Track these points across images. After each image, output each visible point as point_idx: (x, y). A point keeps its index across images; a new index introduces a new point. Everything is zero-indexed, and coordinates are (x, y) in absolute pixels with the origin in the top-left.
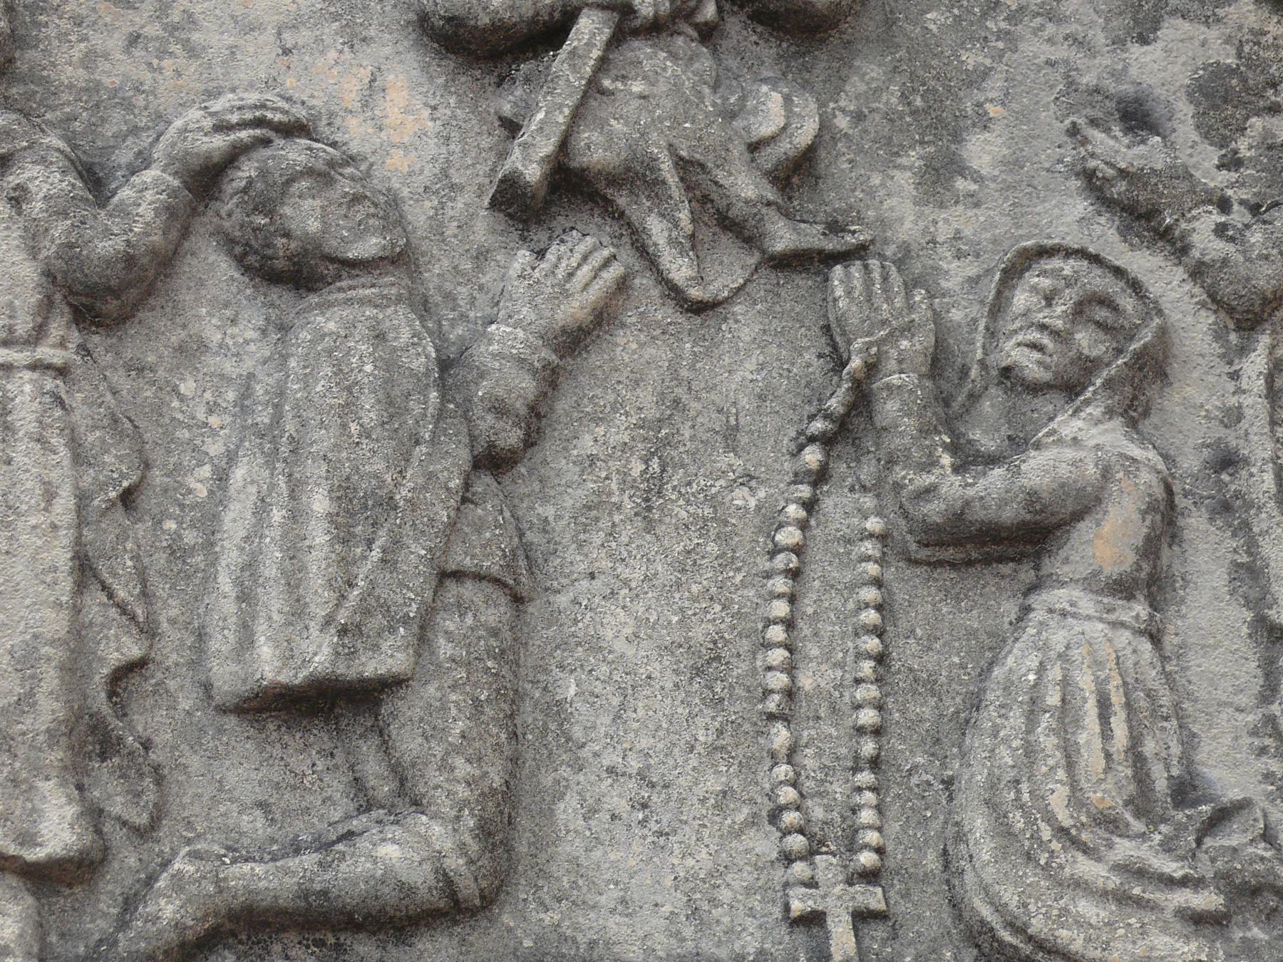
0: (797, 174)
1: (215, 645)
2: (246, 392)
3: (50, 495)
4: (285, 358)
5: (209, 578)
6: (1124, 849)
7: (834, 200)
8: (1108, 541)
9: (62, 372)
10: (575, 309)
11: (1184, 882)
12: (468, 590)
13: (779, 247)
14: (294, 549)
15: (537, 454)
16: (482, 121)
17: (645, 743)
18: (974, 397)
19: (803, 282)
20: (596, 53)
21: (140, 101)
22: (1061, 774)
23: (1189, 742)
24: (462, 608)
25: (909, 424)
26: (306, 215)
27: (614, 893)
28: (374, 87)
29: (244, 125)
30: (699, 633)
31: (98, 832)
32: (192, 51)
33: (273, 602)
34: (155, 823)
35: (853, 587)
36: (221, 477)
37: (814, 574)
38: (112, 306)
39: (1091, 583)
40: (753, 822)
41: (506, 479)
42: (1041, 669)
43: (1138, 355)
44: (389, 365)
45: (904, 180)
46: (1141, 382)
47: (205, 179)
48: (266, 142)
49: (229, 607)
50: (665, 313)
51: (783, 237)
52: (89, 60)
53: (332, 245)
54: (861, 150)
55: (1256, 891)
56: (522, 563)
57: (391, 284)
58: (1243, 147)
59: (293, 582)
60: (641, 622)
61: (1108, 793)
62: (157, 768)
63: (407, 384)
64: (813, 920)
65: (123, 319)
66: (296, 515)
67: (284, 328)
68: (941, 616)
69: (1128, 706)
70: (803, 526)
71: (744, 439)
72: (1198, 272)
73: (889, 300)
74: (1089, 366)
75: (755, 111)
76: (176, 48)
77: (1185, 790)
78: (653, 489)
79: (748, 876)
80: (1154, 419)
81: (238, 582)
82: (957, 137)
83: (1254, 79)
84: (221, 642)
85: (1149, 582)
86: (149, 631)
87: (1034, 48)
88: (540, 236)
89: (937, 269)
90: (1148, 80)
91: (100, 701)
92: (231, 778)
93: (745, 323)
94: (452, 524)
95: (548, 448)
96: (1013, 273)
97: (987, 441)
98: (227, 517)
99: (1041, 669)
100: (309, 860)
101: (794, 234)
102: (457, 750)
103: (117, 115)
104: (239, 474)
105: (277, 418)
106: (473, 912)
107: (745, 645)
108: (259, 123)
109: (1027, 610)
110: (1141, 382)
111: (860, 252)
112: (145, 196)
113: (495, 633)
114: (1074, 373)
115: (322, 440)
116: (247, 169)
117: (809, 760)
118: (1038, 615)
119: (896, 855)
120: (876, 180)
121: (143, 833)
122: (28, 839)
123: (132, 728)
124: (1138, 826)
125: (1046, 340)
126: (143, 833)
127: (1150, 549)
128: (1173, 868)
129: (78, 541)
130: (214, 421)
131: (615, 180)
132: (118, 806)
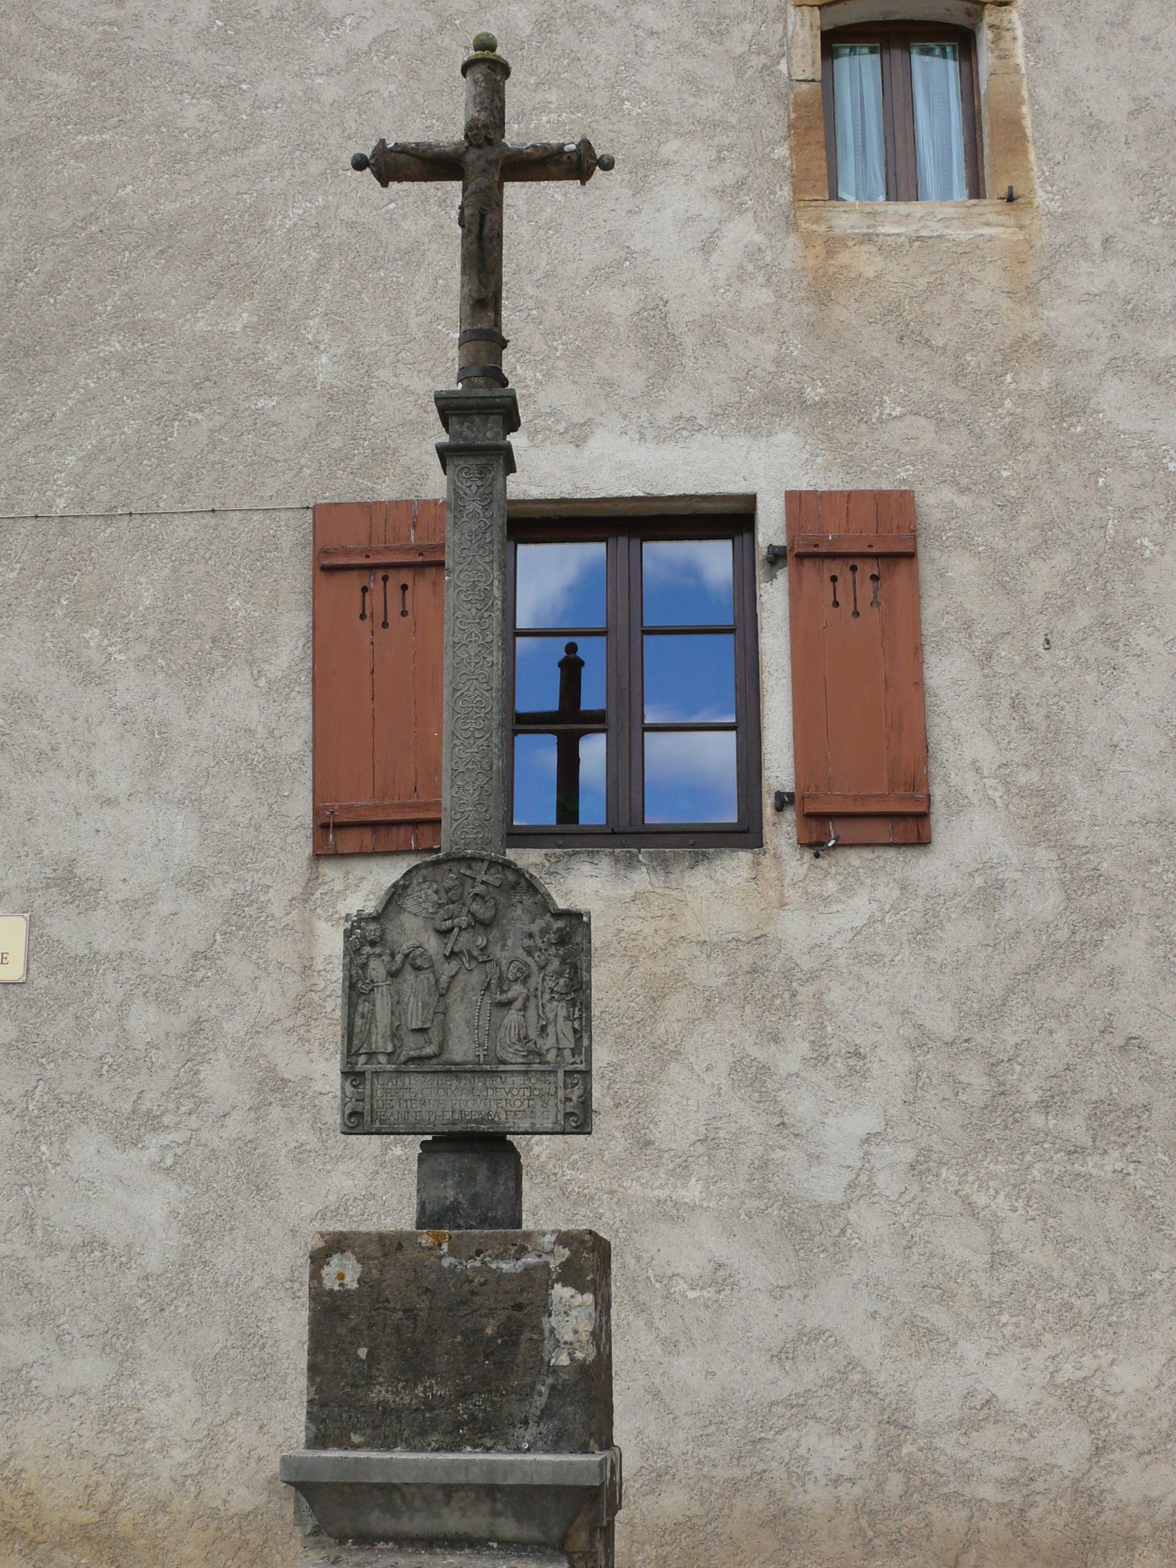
0: (484, 949)
8: (518, 1004)
10: (453, 973)
26: (419, 962)
44: (429, 983)
47: (407, 956)
68: (498, 1013)
85: (524, 1008)
87: (518, 925)
93: (476, 972)
97: (505, 988)
101: (483, 958)
112: (399, 957)
127: (524, 1004)
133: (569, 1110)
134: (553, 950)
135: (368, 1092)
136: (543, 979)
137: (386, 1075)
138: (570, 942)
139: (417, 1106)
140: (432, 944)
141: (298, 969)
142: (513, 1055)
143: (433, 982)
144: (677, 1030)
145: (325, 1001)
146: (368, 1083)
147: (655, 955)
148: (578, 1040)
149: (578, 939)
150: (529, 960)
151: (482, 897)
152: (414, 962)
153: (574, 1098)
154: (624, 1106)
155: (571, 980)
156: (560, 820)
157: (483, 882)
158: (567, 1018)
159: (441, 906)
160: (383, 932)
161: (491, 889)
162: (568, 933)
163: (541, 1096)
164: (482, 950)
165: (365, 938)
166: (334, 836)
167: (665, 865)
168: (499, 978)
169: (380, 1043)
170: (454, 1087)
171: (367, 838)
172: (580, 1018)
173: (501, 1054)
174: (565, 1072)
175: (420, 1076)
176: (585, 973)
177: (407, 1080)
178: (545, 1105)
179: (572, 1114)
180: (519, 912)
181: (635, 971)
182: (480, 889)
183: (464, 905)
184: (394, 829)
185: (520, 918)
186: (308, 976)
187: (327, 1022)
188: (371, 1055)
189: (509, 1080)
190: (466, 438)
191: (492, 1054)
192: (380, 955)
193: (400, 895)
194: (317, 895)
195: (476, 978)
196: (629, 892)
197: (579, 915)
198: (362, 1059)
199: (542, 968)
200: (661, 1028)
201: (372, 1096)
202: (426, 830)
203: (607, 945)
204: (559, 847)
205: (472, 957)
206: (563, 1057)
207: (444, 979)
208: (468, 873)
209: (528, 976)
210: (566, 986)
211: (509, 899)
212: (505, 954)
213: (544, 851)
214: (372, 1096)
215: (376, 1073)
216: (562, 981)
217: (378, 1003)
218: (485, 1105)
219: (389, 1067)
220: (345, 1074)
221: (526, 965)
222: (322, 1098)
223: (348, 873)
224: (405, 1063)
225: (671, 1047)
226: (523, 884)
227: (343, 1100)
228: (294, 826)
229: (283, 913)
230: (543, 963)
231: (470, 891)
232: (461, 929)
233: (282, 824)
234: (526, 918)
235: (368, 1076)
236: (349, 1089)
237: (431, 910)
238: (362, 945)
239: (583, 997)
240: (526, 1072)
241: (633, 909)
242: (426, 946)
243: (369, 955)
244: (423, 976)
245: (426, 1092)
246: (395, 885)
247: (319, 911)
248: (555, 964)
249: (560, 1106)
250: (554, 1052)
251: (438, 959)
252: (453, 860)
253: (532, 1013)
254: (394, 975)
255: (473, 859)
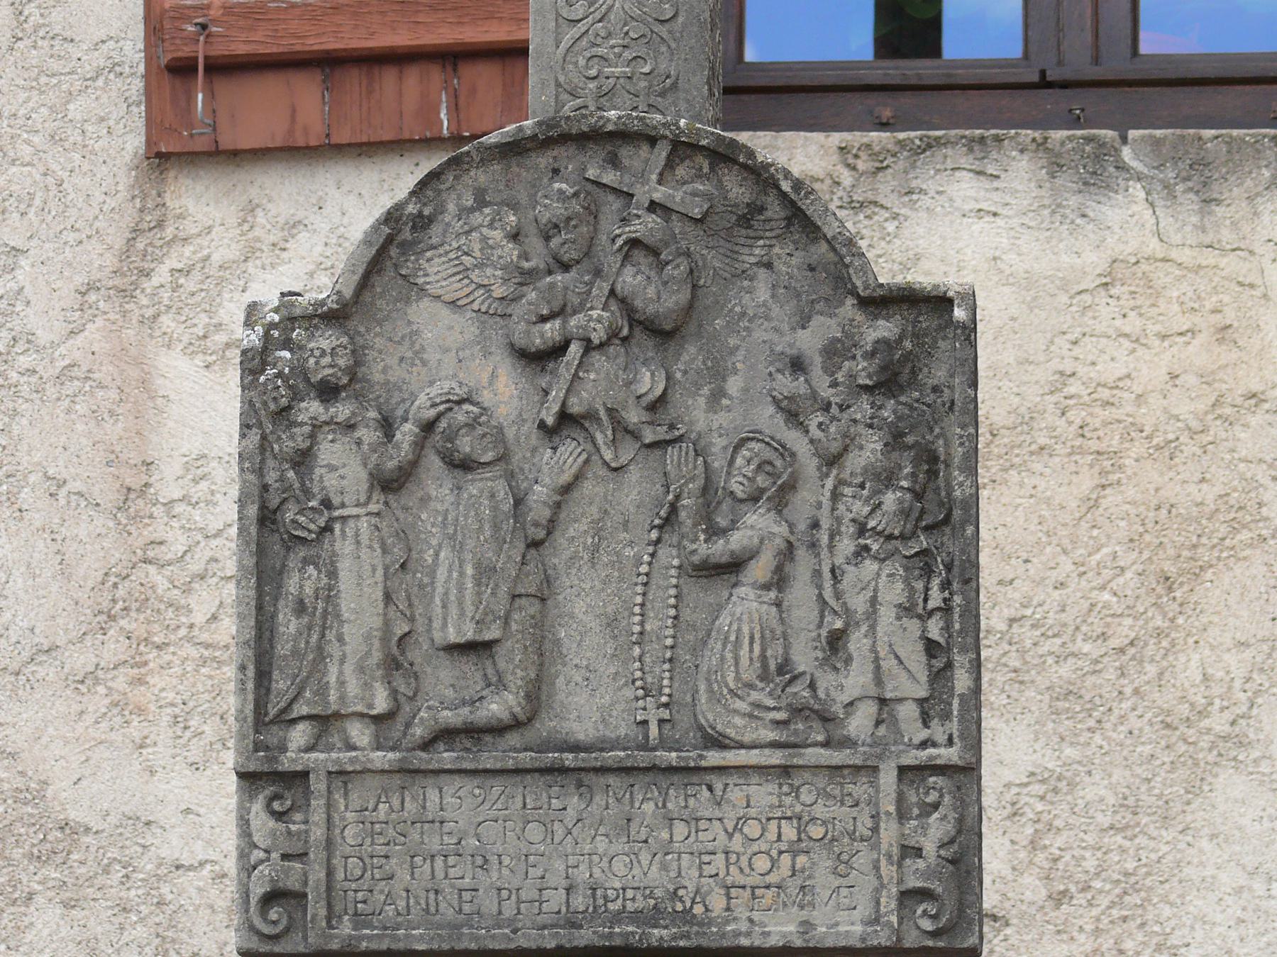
0: (656, 406)
1: (435, 625)
2: (445, 519)
3: (374, 570)
4: (459, 504)
5: (433, 597)
6: (755, 696)
7: (673, 413)
8: (760, 569)
9: (378, 514)
10: (566, 477)
11: (774, 708)
12: (523, 601)
13: (647, 441)
14: (461, 589)
15: (552, 537)
16: (535, 389)
17: (588, 655)
18: (719, 503)
19: (658, 452)
20: (576, 362)
21: (405, 387)
22: (732, 668)
23: (787, 647)
24: (521, 609)
25: (689, 522)
26: (465, 444)
27: (575, 713)
28: (493, 376)
29: (442, 403)
30: (609, 610)
31: (396, 700)
32: (424, 363)
33: (454, 611)
34: (415, 695)
35: (667, 588)
36: (437, 554)
37: (653, 582)
38: (396, 485)
39: (754, 585)
40: (626, 684)
41: (541, 549)
42: (730, 625)
43: (780, 486)
44: (495, 509)
45: (702, 401)
46: (781, 497)
47: (428, 427)
48: (450, 409)
49: (439, 610)
50: (603, 472)
51: (649, 437)
52: (385, 371)
53: (474, 456)
54: (685, 388)
55: (801, 710)
56: (545, 585)
57: (498, 470)
58: (840, 376)
59: (460, 603)
60: (589, 606)
61: (749, 675)
62: (415, 673)
63: (502, 517)
64: (645, 722)
65: (401, 487)
66: (462, 574)
67: (459, 488)
68: (700, 595)
69: (763, 637)
70: (650, 564)
71: (630, 525)
72: (812, 441)
73: (687, 466)
74: (762, 491)
75: (639, 382)
76: (417, 362)
77: (784, 667)
78: (596, 549)
79: (623, 706)
80: (790, 507)
81: (442, 601)
82: (724, 379)
83: (848, 343)
84: (437, 624)
85: (779, 580)
86: (412, 619)
87: (759, 335)
88: (556, 439)
89: (711, 443)
90: (804, 347)
91: (395, 650)
92: (442, 676)
93: (634, 474)
94: (517, 576)
95: (557, 534)
96: (737, 448)
97: (722, 522)
98: (439, 573)
99: (730, 625)
100: (466, 710)
101: (657, 428)
102: (517, 666)
103: (396, 393)
104: (442, 555)
105: (456, 531)
106: (525, 724)
107: (626, 614)
108: (448, 401)
109: (731, 595)
110: (781, 497)
111: (679, 439)
112: (406, 433)
113: (533, 617)
114: (756, 494)
115: (470, 544)
116: (443, 424)
117: (647, 659)
118: (734, 598)
119: (676, 696)
120: (690, 403)
121: (412, 699)
122: (371, 706)
123: (406, 658)
124: (761, 685)
125: (745, 482)
126: (412, 699)
127: (779, 569)
128: (770, 703)
129: (385, 587)
130: (434, 530)
131: (583, 417)
132: (402, 689)
133: (913, 883)
134: (863, 408)
135: (318, 833)
136: (836, 496)
137: (374, 782)
138: (913, 381)
139: (464, 873)
140: (505, 393)
141: (107, 494)
142: (747, 721)
143: (507, 506)
144: (1239, 673)
145: (187, 590)
146: (318, 803)
147: (1170, 449)
148: (940, 676)
149: (939, 374)
150: (793, 438)
151: (654, 252)
152: (449, 444)
153: (930, 848)
154: (1080, 899)
155: (918, 496)
156: (887, 45)
157: (653, 206)
158: (906, 610)
159: (528, 277)
160: (358, 359)
161: (677, 226)
162: (907, 356)
163: (828, 841)
164: (653, 407)
165: (301, 376)
166: (211, 95)
167: (1201, 179)
168: (705, 490)
169: (353, 688)
170: (571, 813)
171: (307, 101)
172: (946, 609)
173: (710, 715)
174: (903, 770)
175: (469, 786)
176: (958, 476)
177: (433, 795)
178: (841, 867)
179: (924, 894)
180: (763, 294)
181: (1111, 499)
182: (646, 226)
183: (598, 273)
184: (388, 77)
185: (765, 317)
186: (135, 518)
187: (194, 652)
188: (325, 721)
189: (736, 795)
190: (506, 494)
191: (684, 720)
192: (350, 427)
193: (405, 247)
194: (161, 275)
195: (636, 492)
196: (1094, 261)
197: (940, 302)
198: (299, 735)
199: (832, 461)
200: (1189, 667)
201: (329, 844)
202: (484, 76)
203: (1027, 421)
204: (884, 126)
205: (623, 431)
206: (894, 721)
207: (540, 494)
208: (609, 177)
209: (789, 487)
210: (905, 513)
211: (733, 255)
212: (721, 419)
213: (836, 138)
214: (329, 844)
215: (341, 775)
216: (890, 500)
217: (344, 566)
218: (664, 867)
219: (382, 759)
220: (248, 778)
221: (784, 451)
222: (183, 879)
223: (251, 208)
224: (426, 745)
225: (1218, 723)
226: (775, 210)
227: (243, 855)
228: (88, 70)
229: (60, 327)
230: (835, 447)
231: (612, 230)
232: (589, 347)
233: (54, 65)
234: (782, 313)
235: (318, 784)
236: (261, 822)
237: (499, 291)
238: (296, 396)
239: (953, 547)
240: (785, 771)
241: (1104, 312)
242: (486, 397)
243: (317, 427)
244: (475, 486)
245: (490, 831)
246: (392, 217)
247: (167, 321)
248: (870, 449)
249: (888, 871)
250: (867, 710)
251: (523, 435)
252: (565, 138)
253: (801, 593)
254: (390, 483)
255: (623, 136)
